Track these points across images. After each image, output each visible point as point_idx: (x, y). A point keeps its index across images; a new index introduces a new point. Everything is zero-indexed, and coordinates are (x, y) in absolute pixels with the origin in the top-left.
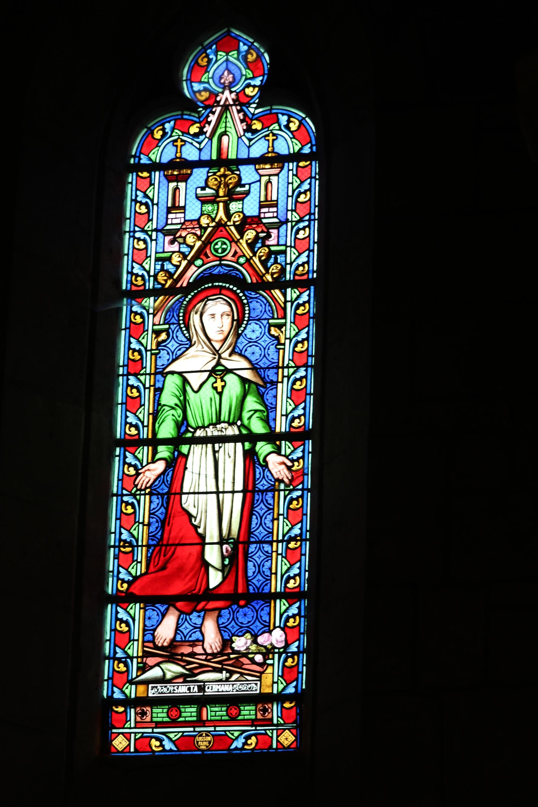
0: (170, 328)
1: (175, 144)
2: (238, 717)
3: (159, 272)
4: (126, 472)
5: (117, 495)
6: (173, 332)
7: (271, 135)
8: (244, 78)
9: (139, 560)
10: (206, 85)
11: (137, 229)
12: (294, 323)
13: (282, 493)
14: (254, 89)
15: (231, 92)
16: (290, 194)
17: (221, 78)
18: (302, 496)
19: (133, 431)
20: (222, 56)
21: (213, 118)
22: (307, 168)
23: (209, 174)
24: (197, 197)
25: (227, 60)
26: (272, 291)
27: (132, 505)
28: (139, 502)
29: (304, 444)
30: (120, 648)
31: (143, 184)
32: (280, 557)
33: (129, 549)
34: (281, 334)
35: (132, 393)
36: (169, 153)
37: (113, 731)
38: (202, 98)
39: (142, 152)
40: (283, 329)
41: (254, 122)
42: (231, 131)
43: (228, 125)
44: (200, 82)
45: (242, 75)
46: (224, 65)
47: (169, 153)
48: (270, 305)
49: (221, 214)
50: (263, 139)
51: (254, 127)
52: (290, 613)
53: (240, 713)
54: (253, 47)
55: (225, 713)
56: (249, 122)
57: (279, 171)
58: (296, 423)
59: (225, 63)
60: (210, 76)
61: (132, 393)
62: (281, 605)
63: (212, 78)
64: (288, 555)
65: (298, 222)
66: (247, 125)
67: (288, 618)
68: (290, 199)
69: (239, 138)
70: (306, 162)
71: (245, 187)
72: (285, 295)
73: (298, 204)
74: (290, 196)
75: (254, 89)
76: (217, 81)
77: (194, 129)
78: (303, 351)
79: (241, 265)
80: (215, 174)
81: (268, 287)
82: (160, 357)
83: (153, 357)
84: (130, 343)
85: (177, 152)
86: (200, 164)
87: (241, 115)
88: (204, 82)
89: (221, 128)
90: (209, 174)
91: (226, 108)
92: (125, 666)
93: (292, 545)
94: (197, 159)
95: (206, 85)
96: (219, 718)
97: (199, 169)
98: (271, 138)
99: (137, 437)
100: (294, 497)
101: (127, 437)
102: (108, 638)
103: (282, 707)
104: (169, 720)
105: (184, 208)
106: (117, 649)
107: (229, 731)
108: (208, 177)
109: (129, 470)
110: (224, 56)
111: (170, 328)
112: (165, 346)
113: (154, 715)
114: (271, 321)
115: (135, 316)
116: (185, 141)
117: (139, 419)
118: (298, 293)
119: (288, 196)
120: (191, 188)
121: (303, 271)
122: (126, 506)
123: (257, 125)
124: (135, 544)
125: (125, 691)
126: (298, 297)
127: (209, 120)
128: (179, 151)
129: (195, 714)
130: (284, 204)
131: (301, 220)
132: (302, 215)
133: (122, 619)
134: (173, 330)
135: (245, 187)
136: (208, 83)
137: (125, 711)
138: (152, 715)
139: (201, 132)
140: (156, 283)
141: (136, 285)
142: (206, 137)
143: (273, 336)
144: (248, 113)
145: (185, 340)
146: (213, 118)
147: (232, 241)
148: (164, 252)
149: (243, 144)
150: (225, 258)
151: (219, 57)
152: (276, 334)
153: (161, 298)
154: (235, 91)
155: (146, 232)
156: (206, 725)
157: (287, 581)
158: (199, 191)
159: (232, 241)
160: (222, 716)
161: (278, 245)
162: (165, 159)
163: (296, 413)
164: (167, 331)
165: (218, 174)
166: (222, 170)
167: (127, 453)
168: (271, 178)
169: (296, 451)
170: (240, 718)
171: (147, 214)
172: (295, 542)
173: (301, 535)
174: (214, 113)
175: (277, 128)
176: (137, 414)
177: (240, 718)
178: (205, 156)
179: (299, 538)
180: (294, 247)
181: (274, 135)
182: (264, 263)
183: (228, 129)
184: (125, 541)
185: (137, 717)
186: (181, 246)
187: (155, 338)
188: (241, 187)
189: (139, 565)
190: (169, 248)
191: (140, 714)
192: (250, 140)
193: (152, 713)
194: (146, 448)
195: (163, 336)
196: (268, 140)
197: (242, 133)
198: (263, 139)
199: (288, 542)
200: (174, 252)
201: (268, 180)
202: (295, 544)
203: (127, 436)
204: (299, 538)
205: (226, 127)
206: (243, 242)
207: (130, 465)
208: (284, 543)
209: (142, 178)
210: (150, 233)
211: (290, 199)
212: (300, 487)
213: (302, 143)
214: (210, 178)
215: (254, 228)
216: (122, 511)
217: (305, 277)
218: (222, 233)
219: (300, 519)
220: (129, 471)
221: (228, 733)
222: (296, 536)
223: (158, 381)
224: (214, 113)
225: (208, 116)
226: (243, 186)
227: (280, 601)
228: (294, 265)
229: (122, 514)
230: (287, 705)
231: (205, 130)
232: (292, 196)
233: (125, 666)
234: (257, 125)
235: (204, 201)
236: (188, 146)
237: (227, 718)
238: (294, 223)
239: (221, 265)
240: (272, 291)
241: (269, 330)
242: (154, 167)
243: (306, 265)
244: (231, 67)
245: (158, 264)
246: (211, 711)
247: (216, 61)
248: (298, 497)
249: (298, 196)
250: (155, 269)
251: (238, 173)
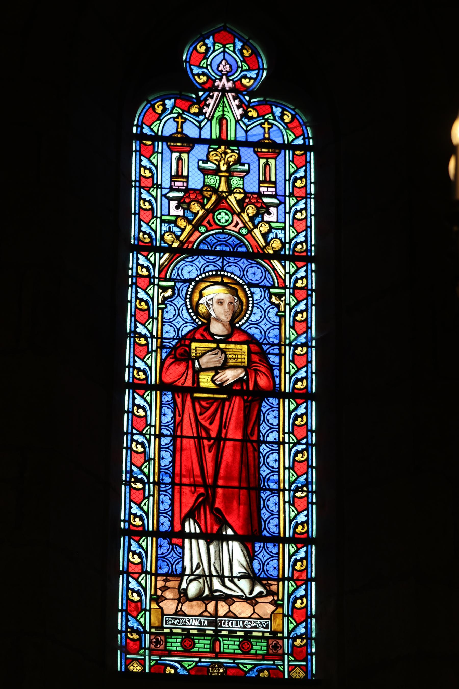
0: (175, 285)
1: (176, 120)
2: (250, 651)
3: (165, 233)
4: (143, 174)
5: (127, 433)
6: (179, 290)
7: (266, 123)
8: (240, 69)
9: (153, 424)
10: (205, 70)
11: (134, 431)
12: (293, 161)
13: (287, 445)
14: (250, 81)
15: (228, 80)
16: (287, 178)
17: (218, 66)
18: (306, 449)
19: (138, 522)
20: (219, 47)
21: (211, 102)
22: (303, 427)
23: (210, 150)
24: (200, 169)
25: (224, 52)
26: (272, 261)
27: (142, 444)
28: (149, 441)
29: (307, 266)
30: (136, 466)
31: (137, 496)
32: (287, 505)
33: (139, 486)
34: (281, 303)
35: (135, 522)
36: (171, 128)
37: (127, 657)
38: (201, 81)
39: (144, 121)
40: (283, 299)
41: (250, 109)
42: (229, 116)
43: (225, 109)
44: (200, 67)
45: (238, 67)
46: (221, 56)
47: (171, 128)
48: (269, 273)
49: (223, 187)
50: (259, 126)
51: (250, 114)
52: (298, 557)
53: (252, 647)
54: (248, 43)
55: (237, 647)
56: (245, 108)
57: (276, 156)
58: (299, 385)
59: (222, 54)
60: (209, 63)
61: (142, 272)
62: (290, 548)
63: (210, 65)
64: (295, 160)
65: (295, 445)
66: (243, 110)
67: (297, 525)
68: (287, 183)
69: (237, 122)
70: (301, 151)
71: (244, 166)
72: (284, 267)
73: (296, 356)
74: (287, 180)
75: (250, 81)
76: (215, 68)
77: (194, 109)
78: (302, 569)
79: (243, 236)
80: (215, 150)
81: (269, 257)
82: (167, 312)
83: (160, 311)
84: (130, 508)
85: (178, 128)
86: (200, 141)
87: (237, 102)
88: (202, 67)
89: (219, 111)
90: (210, 150)
91: (224, 91)
92: (149, 205)
93: (298, 642)
94: (197, 136)
95: (205, 70)
96: (232, 651)
97: (199, 145)
98: (266, 126)
99: (144, 382)
100: (300, 449)
101: (136, 381)
102: (130, 267)
103: (294, 154)
104: (183, 650)
105: (187, 177)
106: (132, 504)
107: (242, 664)
108: (209, 152)
109: (141, 304)
110: (221, 48)
111: (175, 285)
112: (171, 301)
113: (169, 644)
114: (272, 290)
115: (134, 519)
116: (186, 119)
117: (151, 228)
118: (296, 201)
119: (285, 180)
120: (194, 162)
121: (301, 249)
122: (138, 409)
123: (253, 113)
124: (146, 481)
125: (146, 398)
126: (296, 552)
127: (207, 103)
128: (179, 126)
129: (208, 646)
130: (282, 189)
131: (299, 443)
132: (300, 437)
133: (134, 589)
134: (178, 287)
135: (244, 166)
136: (207, 68)
137: (153, 144)
138: (166, 645)
139: (201, 113)
140: (162, 242)
141: (143, 242)
142: (205, 118)
143: (273, 304)
144: (244, 101)
145: (189, 318)
146: (211, 102)
147: (233, 212)
148: (169, 215)
149: (241, 128)
150: (227, 228)
151: (216, 48)
152: (277, 302)
153: (167, 255)
154: (232, 80)
155: (144, 435)
156: (219, 656)
157: (296, 383)
158: (201, 163)
159: (233, 212)
160: (234, 650)
161: (277, 222)
162: (167, 133)
163: (299, 275)
164: (173, 288)
165: (219, 150)
166: (223, 147)
167: (132, 541)
168: (269, 160)
169: (299, 271)
170: (253, 652)
171: (151, 179)
172: (300, 640)
173: (306, 633)
174: (212, 97)
175: (272, 118)
176: (150, 224)
177: (253, 652)
178: (205, 135)
179: (304, 636)
180: (293, 433)
181: (269, 124)
182: (265, 236)
183: (225, 113)
184: (132, 628)
185: (151, 645)
186: (186, 211)
187: (161, 293)
188: (240, 165)
189: (155, 321)
190: (174, 212)
191: (154, 642)
192: (247, 126)
193: (166, 642)
194: (150, 539)
195: (169, 293)
196: (264, 128)
197: (239, 118)
198: (259, 126)
199: (294, 639)
200: (178, 217)
201: (266, 163)
202: (301, 642)
203: (131, 526)
204: (304, 636)
205: (223, 111)
206: (244, 215)
207: (134, 553)
208: (292, 348)
209: (135, 489)
210: (148, 437)
211: (287, 183)
212: (304, 441)
213: (297, 365)
214: (211, 153)
215: (254, 203)
216: (140, 175)
217: (304, 254)
218: (224, 204)
219: (305, 435)
220: (145, 173)
221: (240, 665)
222: (302, 634)
223: (163, 502)
224: (212, 97)
225: (206, 99)
226: (243, 165)
227: (289, 401)
228: (292, 213)
229: (141, 178)
230: (298, 152)
231: (204, 111)
232: (289, 180)
233: (149, 205)
234: (253, 113)
235: (205, 172)
236: (188, 123)
237: (239, 651)
238: (291, 445)
239: (223, 233)
240: (272, 261)
241: (270, 298)
242: (156, 138)
243: (304, 244)
244: (227, 56)
245: (165, 226)
246: (223, 644)
247: (214, 51)
248: (303, 450)
249: (295, 213)
250: (161, 230)
251: (237, 152)
